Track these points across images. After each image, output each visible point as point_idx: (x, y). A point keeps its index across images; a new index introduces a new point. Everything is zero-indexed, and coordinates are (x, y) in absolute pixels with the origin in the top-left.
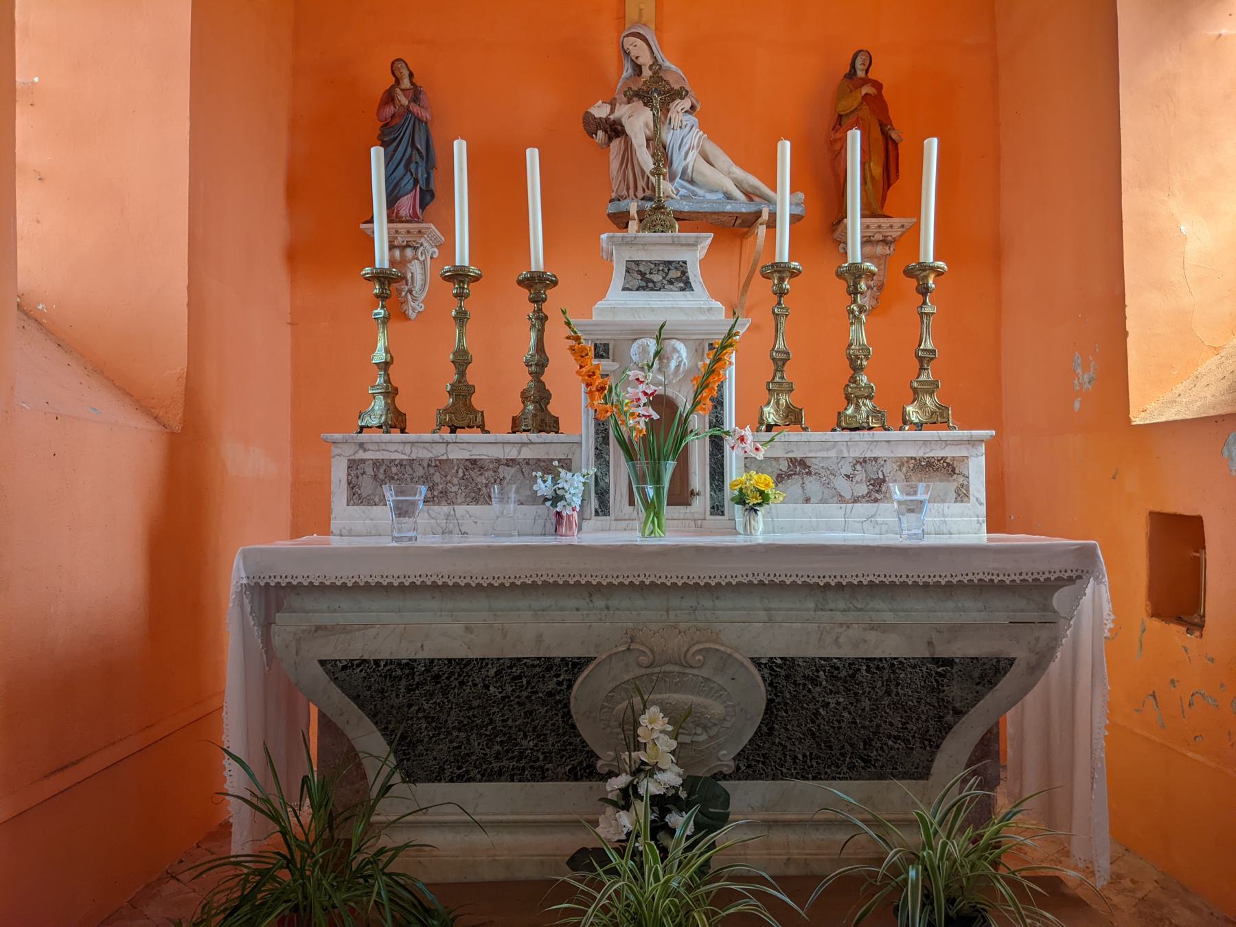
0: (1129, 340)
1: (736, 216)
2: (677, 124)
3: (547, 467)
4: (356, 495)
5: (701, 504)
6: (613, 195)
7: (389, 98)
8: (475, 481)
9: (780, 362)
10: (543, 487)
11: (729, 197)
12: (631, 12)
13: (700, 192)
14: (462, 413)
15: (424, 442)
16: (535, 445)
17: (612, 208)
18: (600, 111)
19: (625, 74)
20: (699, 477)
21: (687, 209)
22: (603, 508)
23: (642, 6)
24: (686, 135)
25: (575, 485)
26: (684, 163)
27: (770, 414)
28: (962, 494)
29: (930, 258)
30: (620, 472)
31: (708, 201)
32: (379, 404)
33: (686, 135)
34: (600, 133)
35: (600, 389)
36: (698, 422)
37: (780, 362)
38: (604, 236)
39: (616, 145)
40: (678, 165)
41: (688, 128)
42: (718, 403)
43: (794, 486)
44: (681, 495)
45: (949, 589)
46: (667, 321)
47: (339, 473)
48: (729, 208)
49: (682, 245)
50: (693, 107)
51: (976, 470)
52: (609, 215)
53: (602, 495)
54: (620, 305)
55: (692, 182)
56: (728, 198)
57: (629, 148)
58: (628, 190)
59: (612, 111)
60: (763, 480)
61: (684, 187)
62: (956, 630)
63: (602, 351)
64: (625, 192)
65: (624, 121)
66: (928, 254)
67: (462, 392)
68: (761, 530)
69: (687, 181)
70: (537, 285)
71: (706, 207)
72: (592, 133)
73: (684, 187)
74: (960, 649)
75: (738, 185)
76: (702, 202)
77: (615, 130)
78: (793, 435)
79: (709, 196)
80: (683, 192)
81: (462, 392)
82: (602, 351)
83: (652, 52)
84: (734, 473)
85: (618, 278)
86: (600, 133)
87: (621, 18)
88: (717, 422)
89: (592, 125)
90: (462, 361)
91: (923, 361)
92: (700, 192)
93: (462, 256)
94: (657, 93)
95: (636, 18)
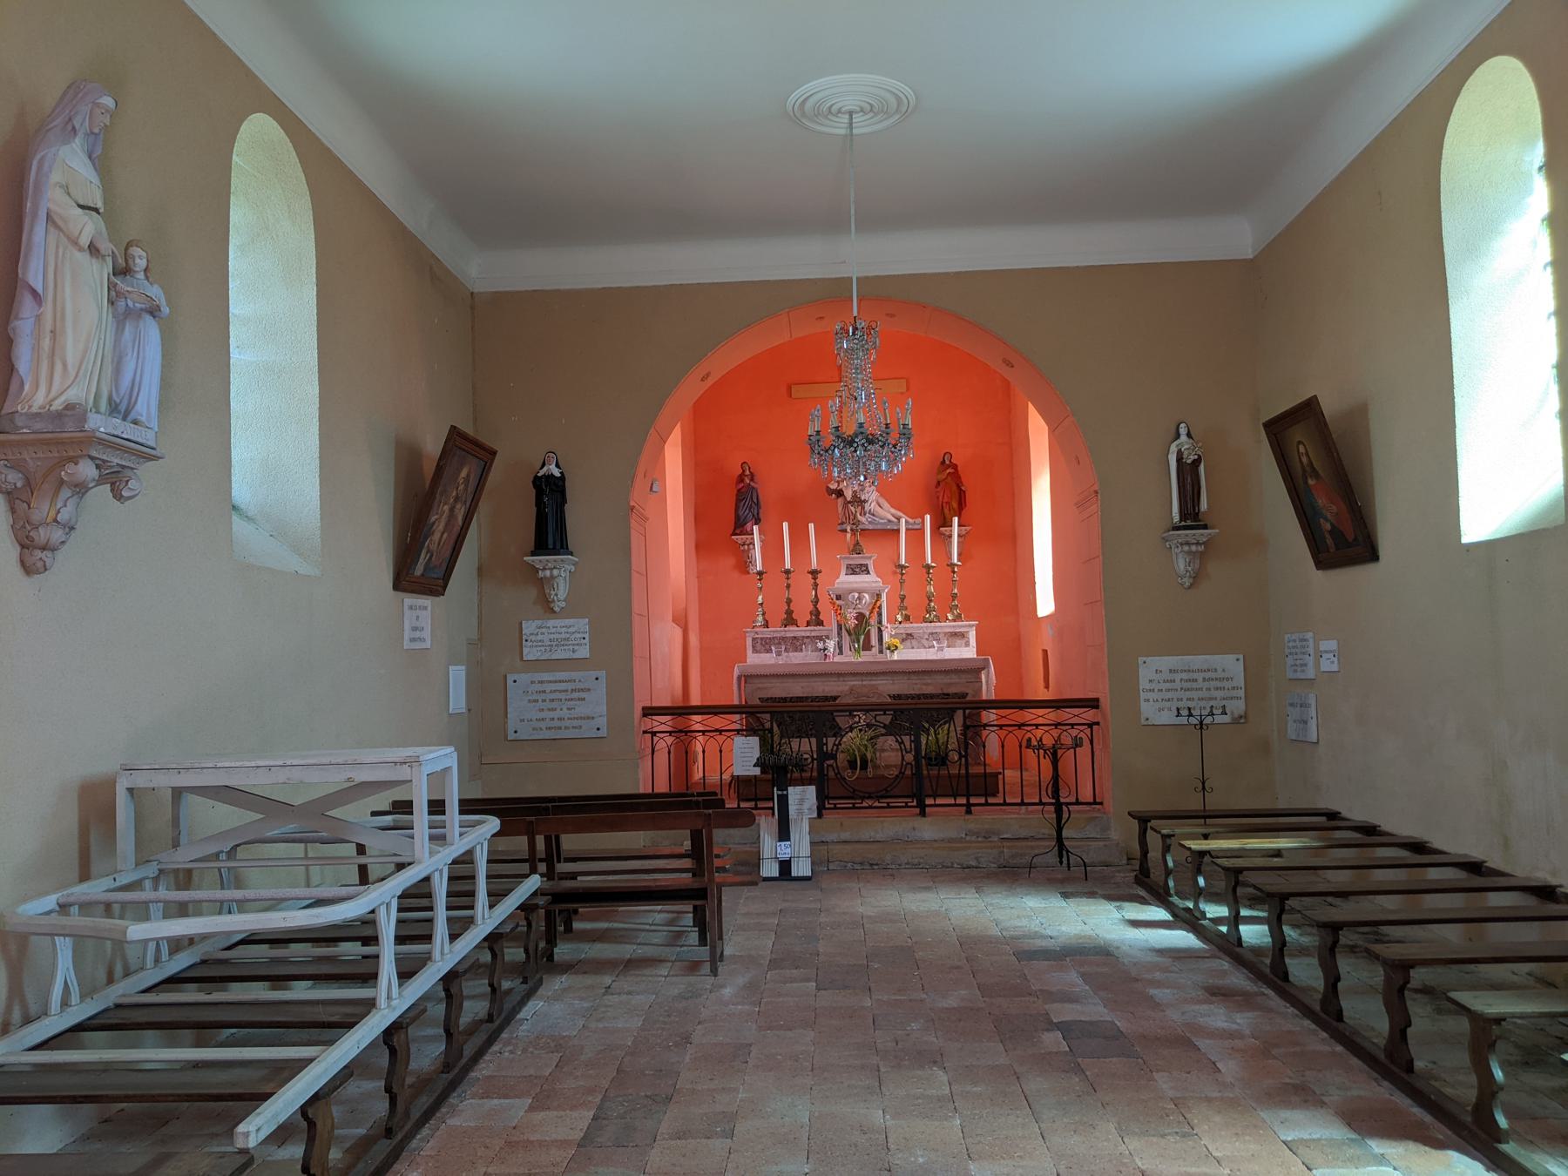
0: (1550, 352)
3: (820, 638)
4: (755, 650)
5: (875, 650)
7: (741, 479)
8: (796, 644)
9: (903, 598)
10: (820, 645)
14: (790, 620)
15: (776, 631)
16: (815, 631)
20: (874, 641)
22: (841, 653)
25: (831, 644)
27: (899, 618)
28: (967, 645)
29: (955, 560)
30: (846, 639)
32: (760, 618)
35: (838, 610)
36: (874, 621)
37: (903, 598)
42: (880, 615)
43: (908, 643)
44: (867, 646)
45: (946, 672)
46: (864, 585)
47: (749, 642)
51: (972, 635)
53: (840, 648)
54: (845, 580)
60: (896, 642)
62: (950, 684)
63: (839, 597)
66: (955, 560)
67: (789, 613)
68: (896, 657)
70: (814, 573)
74: (952, 690)
78: (908, 625)
81: (789, 613)
82: (839, 597)
84: (886, 638)
85: (843, 571)
88: (880, 622)
89: (830, 492)
90: (789, 601)
91: (954, 597)
93: (788, 565)
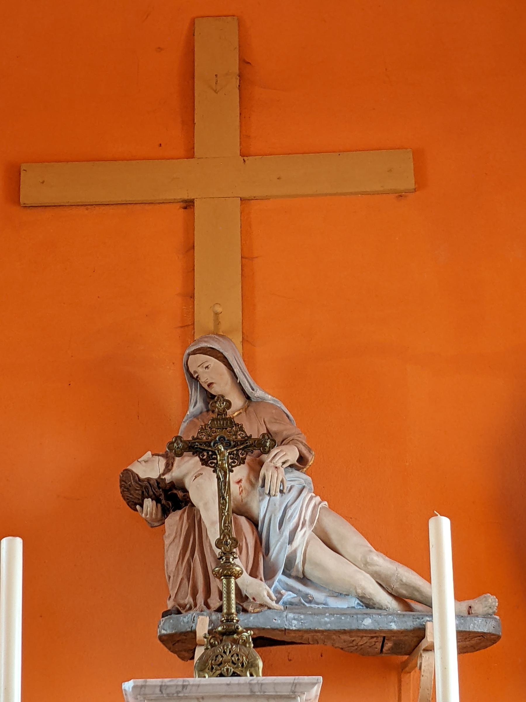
1: (384, 636)
2: (275, 487)
6: (170, 604)
11: (368, 604)
12: (203, 317)
13: (318, 596)
17: (166, 627)
18: (149, 468)
19: (192, 410)
21: (295, 625)
23: (219, 309)
24: (292, 506)
26: (289, 549)
31: (332, 611)
33: (292, 506)
34: (149, 503)
38: (128, 686)
39: (175, 521)
40: (279, 552)
41: (294, 493)
48: (368, 623)
49: (414, 649)
50: (302, 460)
52: (163, 639)
55: (304, 579)
56: (368, 606)
57: (195, 523)
58: (194, 595)
59: (168, 468)
61: (290, 589)
64: (189, 599)
65: (189, 483)
69: (297, 578)
71: (327, 623)
72: (135, 503)
73: (290, 589)
75: (384, 583)
76: (321, 613)
77: (173, 497)
79: (334, 603)
80: (288, 596)
83: (235, 376)
86: (149, 503)
87: (188, 325)
89: (135, 491)
92: (318, 596)
94: (224, 440)
95: (211, 326)
